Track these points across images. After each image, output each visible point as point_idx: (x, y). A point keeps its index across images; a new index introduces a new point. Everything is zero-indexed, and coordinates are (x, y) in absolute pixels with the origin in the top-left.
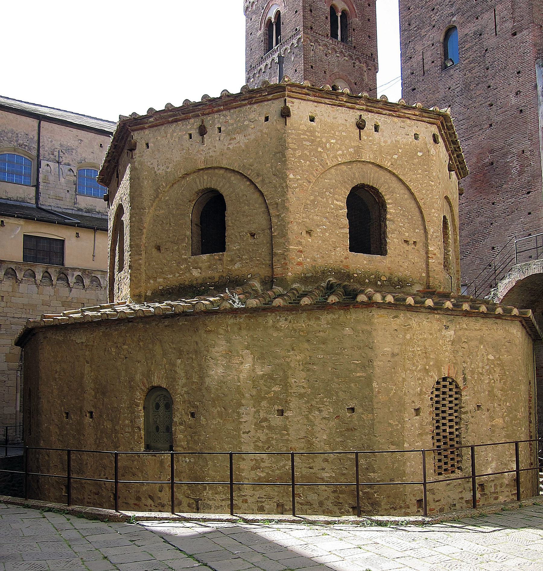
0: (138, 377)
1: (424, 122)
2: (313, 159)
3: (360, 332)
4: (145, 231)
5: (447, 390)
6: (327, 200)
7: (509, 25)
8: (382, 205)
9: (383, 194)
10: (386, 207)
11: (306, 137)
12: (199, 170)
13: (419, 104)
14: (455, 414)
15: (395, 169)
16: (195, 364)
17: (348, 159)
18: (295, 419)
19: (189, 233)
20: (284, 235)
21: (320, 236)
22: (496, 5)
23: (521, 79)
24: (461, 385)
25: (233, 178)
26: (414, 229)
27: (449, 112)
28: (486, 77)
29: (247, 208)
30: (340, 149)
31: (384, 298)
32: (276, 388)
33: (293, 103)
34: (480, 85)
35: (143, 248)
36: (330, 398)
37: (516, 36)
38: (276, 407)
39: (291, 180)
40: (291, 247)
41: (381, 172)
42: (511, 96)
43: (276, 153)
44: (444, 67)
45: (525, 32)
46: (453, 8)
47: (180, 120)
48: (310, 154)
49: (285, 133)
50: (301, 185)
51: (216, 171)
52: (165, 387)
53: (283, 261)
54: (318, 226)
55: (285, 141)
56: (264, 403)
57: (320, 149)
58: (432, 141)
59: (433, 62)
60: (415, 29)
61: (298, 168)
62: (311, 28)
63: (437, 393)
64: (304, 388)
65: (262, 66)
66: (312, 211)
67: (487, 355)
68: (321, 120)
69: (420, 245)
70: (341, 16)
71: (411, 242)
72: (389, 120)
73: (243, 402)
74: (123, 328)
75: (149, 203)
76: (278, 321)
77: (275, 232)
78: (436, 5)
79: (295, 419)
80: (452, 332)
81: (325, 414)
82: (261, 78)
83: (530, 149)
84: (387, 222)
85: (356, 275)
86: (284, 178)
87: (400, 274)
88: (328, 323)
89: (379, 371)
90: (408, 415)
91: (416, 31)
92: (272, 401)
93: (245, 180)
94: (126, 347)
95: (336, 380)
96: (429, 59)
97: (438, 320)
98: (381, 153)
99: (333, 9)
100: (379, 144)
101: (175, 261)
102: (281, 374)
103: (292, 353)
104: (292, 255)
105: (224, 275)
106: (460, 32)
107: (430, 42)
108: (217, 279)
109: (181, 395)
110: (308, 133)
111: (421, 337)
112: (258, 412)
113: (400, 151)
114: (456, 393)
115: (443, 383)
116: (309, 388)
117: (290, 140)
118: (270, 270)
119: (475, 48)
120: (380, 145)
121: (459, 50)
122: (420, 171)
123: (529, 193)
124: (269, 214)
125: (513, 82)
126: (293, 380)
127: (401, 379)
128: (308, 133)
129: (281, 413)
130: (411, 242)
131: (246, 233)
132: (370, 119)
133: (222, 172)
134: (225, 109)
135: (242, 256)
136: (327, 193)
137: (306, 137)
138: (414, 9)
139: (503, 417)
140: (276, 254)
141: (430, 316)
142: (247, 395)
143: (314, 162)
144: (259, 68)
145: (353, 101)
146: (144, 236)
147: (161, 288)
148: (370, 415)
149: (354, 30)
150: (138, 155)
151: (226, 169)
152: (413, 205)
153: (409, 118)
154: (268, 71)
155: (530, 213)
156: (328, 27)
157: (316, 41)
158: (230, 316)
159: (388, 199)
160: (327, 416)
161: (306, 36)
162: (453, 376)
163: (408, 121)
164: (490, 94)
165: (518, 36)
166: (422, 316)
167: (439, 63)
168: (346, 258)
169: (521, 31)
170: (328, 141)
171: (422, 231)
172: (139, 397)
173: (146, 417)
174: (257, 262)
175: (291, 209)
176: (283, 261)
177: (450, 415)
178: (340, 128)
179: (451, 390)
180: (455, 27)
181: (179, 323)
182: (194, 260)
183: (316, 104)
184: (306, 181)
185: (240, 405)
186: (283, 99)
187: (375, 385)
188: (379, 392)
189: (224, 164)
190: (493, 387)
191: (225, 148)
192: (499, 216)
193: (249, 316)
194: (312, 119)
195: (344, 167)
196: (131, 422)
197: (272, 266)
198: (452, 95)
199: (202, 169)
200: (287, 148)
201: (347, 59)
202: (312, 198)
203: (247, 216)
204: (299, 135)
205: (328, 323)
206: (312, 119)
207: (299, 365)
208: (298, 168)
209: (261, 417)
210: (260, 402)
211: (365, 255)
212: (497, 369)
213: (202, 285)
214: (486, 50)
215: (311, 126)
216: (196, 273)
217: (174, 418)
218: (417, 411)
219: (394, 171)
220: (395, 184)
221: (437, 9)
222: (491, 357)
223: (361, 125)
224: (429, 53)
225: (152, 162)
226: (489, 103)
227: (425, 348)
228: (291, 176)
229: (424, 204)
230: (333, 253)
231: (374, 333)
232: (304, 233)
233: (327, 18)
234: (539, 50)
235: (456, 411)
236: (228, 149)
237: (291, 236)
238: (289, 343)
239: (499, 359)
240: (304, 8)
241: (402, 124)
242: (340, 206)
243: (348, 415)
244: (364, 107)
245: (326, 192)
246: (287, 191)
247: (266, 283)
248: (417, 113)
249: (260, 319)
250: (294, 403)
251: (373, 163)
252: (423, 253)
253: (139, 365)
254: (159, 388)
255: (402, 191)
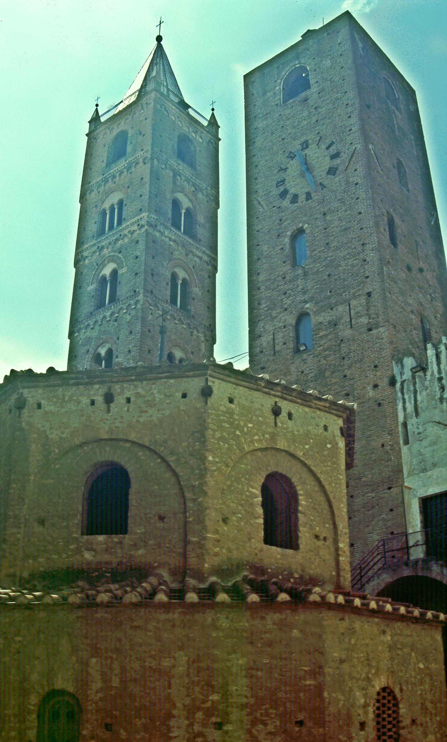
0: (34, 677)
1: (333, 414)
2: (232, 442)
3: (309, 634)
4: (27, 500)
5: (385, 701)
6: (243, 486)
7: (364, 320)
8: (294, 496)
9: (295, 484)
10: (298, 499)
11: (225, 418)
12: (101, 440)
13: (330, 397)
14: (394, 730)
15: (307, 459)
16: (116, 665)
17: (264, 445)
18: (236, 734)
19: (80, 508)
20: (201, 521)
21: (235, 525)
22: (350, 300)
23: (378, 374)
24: (399, 696)
25: (140, 454)
26: (324, 523)
27: (355, 406)
28: (342, 367)
29: (156, 487)
30: (257, 434)
31: (336, 598)
32: (215, 697)
33: (213, 382)
34: (336, 374)
35: (22, 520)
36: (276, 709)
37: (371, 332)
38: (214, 719)
39: (210, 462)
40: (209, 535)
41: (294, 461)
42: (369, 388)
43: (194, 432)
44: (297, 351)
45: (381, 330)
46: (306, 296)
47: (81, 384)
48: (229, 437)
49: (205, 413)
50: (219, 469)
51: (121, 443)
52: (71, 691)
53: (199, 551)
54: (234, 513)
55: (205, 421)
56: (199, 715)
57: (238, 433)
58: (339, 434)
59: (285, 344)
60: (265, 309)
61: (217, 450)
62: (152, 292)
63: (377, 705)
64: (246, 697)
65: (91, 322)
66: (229, 497)
67: (418, 663)
68: (239, 403)
69: (329, 542)
70: (181, 284)
71: (322, 537)
72: (301, 409)
73: (175, 712)
74: (17, 615)
75: (36, 470)
76: (218, 619)
77: (190, 517)
78: (288, 290)
79: (236, 734)
80: (389, 638)
81: (271, 728)
82: (88, 334)
83: (390, 443)
84: (299, 515)
85: (270, 571)
86: (203, 459)
87: (312, 572)
88: (274, 624)
89: (329, 679)
90: (355, 729)
91: (266, 311)
92: (209, 713)
93: (155, 456)
94: (18, 639)
95: (283, 688)
96: (281, 340)
97: (377, 624)
98: (294, 441)
99: (174, 276)
100: (292, 432)
101: (63, 539)
102: (220, 680)
103: (233, 656)
104: (209, 545)
105: (124, 561)
106: (314, 320)
107: (281, 324)
108: (114, 565)
109: (94, 703)
110: (227, 415)
111: (364, 642)
112: (191, 725)
113: (311, 441)
114: (394, 705)
115: (382, 694)
116: (252, 697)
117: (209, 421)
118: (182, 559)
119: (330, 337)
120: (294, 434)
121: (313, 336)
122: (329, 463)
123: (390, 488)
124: (184, 497)
125: (370, 374)
126: (234, 688)
127: (348, 689)
128: (227, 415)
129: (219, 726)
130: (322, 537)
131: (155, 516)
132: (285, 406)
133: (128, 445)
134: (136, 380)
135: (148, 540)
136: (243, 479)
137: (225, 418)
138: (265, 290)
139: (435, 733)
140: (189, 542)
141: (370, 619)
142: (179, 705)
143: (232, 445)
144: (86, 323)
145: (270, 387)
146: (26, 506)
147: (42, 569)
148: (321, 730)
149: (193, 299)
150: (26, 414)
151: (134, 443)
152: (322, 498)
153: (319, 409)
154: (97, 327)
155: (391, 510)
156: (168, 292)
157: (156, 306)
158: (162, 611)
159: (300, 490)
160: (273, 730)
161: (145, 299)
162: (391, 685)
163: (318, 412)
164: (347, 383)
165: (374, 332)
166: (364, 619)
167: (291, 345)
168: (261, 551)
169: (377, 328)
170: (246, 425)
171: (332, 526)
172: (34, 700)
173: (40, 728)
174: (167, 549)
175: (210, 493)
176: (199, 551)
177: (390, 730)
178: (257, 413)
179: (389, 702)
180: (307, 314)
181: (96, 615)
182: (87, 541)
183: (235, 386)
184: (224, 465)
185: (170, 716)
186: (203, 379)
187: (326, 694)
188: (329, 703)
189: (133, 436)
190: (425, 699)
191: (134, 420)
192: (358, 511)
193: (183, 612)
194: (231, 401)
195: (259, 454)
196: (20, 733)
197: (184, 555)
198: (305, 378)
199: (105, 440)
200: (207, 429)
201: (185, 326)
202: (229, 483)
203: (156, 497)
204: (218, 416)
205: (274, 624)
206: (231, 401)
207: (241, 670)
208: (217, 450)
209: (196, 731)
210: (194, 713)
211: (279, 549)
212: (427, 680)
213: (97, 570)
214: (342, 340)
215: (230, 408)
216: (88, 556)
217: (83, 730)
218: (363, 725)
219: (306, 462)
220: (306, 475)
221: (290, 294)
222: (421, 666)
223: (276, 412)
224: (281, 335)
225: (43, 424)
226: (346, 392)
227: (368, 654)
228: (210, 458)
229: (334, 498)
230: (248, 545)
231: (324, 636)
232: (221, 520)
233: (167, 284)
234: (394, 348)
235: (394, 726)
236: (138, 421)
237: (208, 523)
238: (230, 644)
239: (427, 668)
240: (146, 271)
241: (313, 414)
242: (255, 494)
243: (297, 729)
244: (280, 394)
245: (242, 477)
246: (206, 473)
247: (175, 574)
248: (327, 405)
249: (198, 617)
250: (235, 714)
251: (286, 452)
252: (332, 549)
253: (36, 662)
254: (62, 692)
255: (313, 483)
